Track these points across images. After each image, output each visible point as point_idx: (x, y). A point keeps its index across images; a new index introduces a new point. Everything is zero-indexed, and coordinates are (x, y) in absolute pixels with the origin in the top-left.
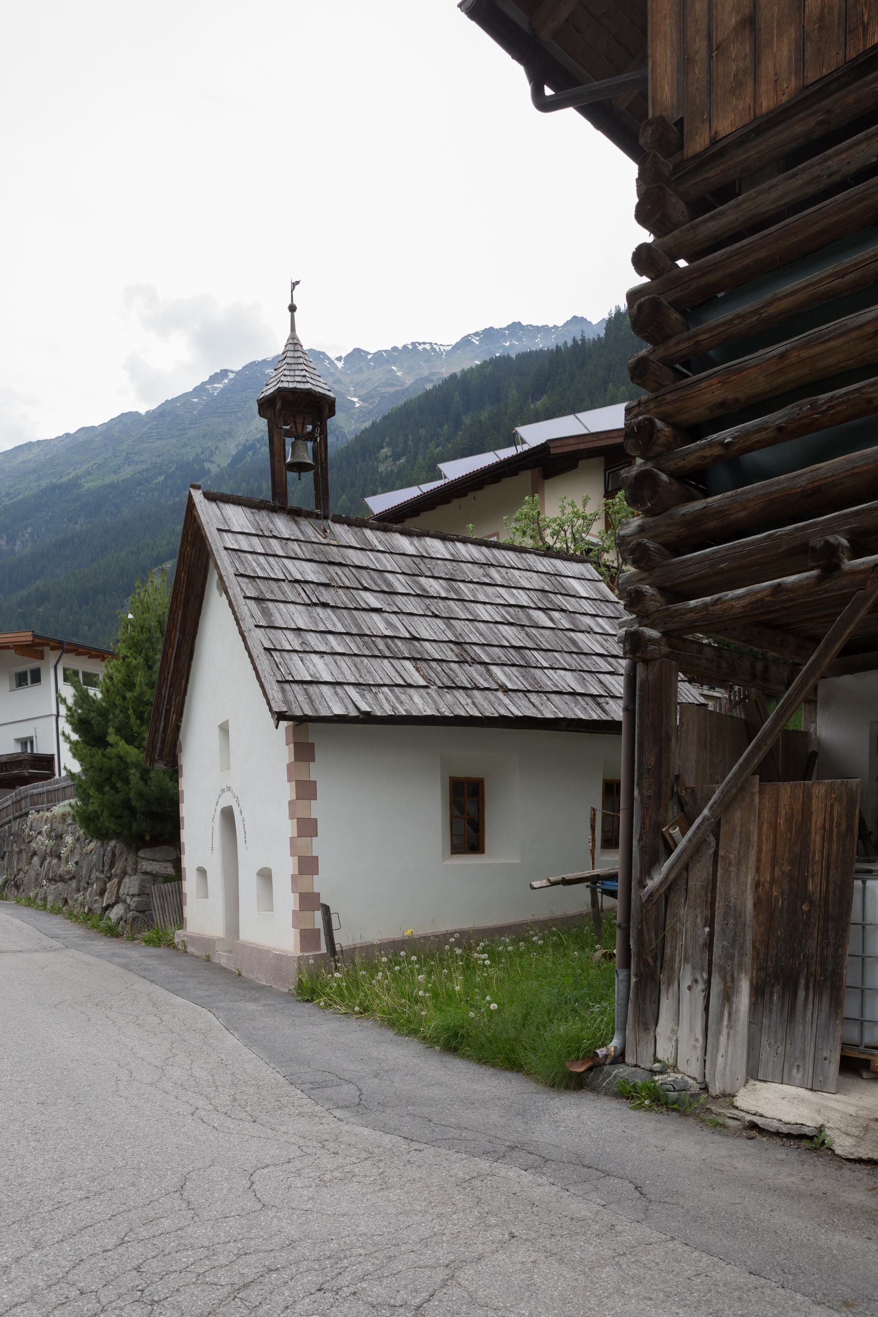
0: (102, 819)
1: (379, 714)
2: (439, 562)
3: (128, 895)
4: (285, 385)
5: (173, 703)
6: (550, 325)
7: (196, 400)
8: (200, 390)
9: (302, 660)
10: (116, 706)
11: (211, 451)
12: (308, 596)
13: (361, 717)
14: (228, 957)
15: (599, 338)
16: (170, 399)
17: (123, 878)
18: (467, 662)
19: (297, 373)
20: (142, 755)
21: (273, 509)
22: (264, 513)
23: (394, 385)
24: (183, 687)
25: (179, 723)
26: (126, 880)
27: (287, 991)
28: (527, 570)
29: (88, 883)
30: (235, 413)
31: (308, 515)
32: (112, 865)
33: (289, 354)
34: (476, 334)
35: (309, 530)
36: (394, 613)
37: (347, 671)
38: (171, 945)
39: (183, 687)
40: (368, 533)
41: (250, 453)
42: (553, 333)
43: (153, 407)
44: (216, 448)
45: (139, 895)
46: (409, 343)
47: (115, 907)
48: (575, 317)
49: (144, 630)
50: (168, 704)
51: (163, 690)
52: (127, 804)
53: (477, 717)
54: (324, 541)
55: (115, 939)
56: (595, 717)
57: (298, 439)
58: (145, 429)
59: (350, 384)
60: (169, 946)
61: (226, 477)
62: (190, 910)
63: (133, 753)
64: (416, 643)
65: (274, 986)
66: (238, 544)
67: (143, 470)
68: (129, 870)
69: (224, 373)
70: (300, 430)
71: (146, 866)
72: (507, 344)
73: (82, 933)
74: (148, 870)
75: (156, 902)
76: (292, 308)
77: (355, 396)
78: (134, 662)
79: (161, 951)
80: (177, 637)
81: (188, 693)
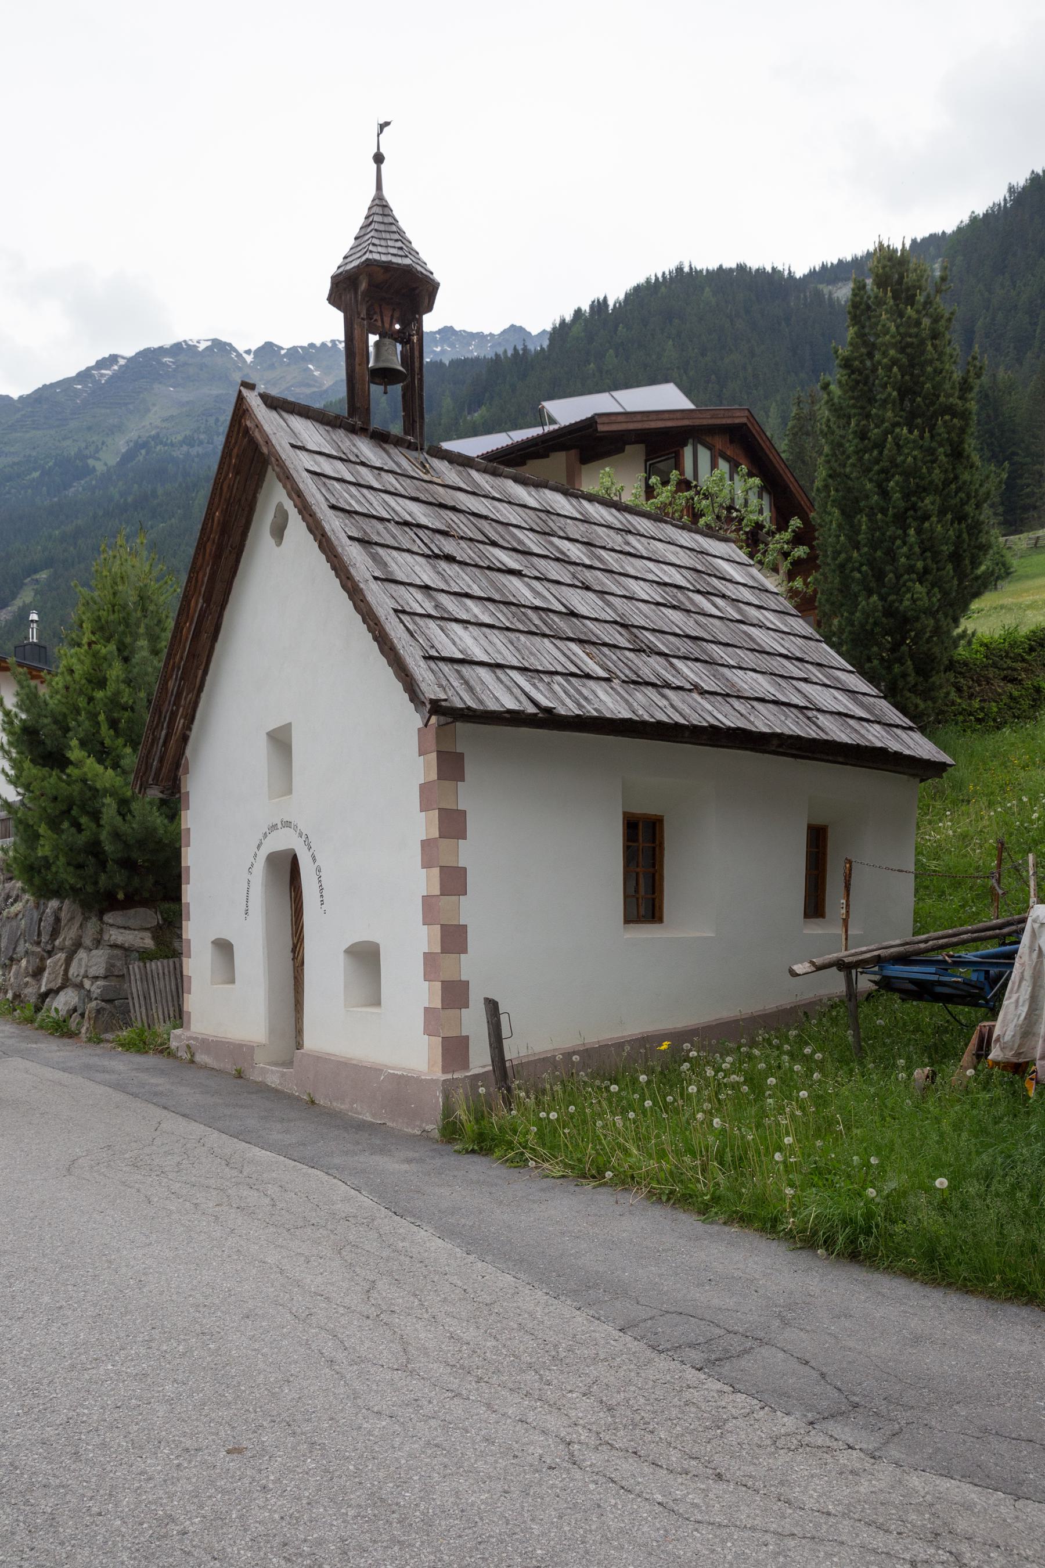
0: (54, 869)
1: (563, 713)
2: (569, 521)
3: (86, 976)
4: (376, 257)
5: (183, 702)
6: (486, 332)
7: (79, 387)
8: (84, 376)
9: (442, 630)
10: (78, 712)
12: (426, 544)
13: (540, 715)
14: (283, 1075)
15: (542, 349)
16: (48, 383)
17: (75, 952)
18: (644, 651)
19: (390, 243)
20: (118, 778)
21: (352, 430)
22: (341, 433)
23: (308, 385)
24: (198, 680)
25: (188, 732)
26: (82, 954)
27: (419, 1133)
28: (669, 543)
29: (11, 959)
31: (398, 442)
32: (55, 933)
33: (377, 218)
35: (402, 460)
36: (536, 578)
37: (500, 649)
38: (164, 1050)
39: (198, 680)
40: (474, 473)
41: (143, 452)
42: (489, 341)
43: (27, 390)
44: (103, 443)
45: (105, 977)
47: (62, 993)
48: (513, 326)
50: (174, 704)
51: (171, 684)
52: (94, 848)
53: (683, 725)
54: (426, 477)
55: (67, 1040)
56: (815, 736)
58: (18, 416)
60: (161, 1052)
61: (114, 477)
62: (192, 1002)
63: (105, 777)
64: (575, 620)
65: (389, 1124)
66: (319, 466)
67: (14, 464)
68: (87, 941)
69: (114, 358)
70: (387, 325)
72: (438, 349)
73: (12, 1030)
74: (119, 942)
75: (135, 987)
76: (379, 159)
78: (104, 651)
79: (150, 1060)
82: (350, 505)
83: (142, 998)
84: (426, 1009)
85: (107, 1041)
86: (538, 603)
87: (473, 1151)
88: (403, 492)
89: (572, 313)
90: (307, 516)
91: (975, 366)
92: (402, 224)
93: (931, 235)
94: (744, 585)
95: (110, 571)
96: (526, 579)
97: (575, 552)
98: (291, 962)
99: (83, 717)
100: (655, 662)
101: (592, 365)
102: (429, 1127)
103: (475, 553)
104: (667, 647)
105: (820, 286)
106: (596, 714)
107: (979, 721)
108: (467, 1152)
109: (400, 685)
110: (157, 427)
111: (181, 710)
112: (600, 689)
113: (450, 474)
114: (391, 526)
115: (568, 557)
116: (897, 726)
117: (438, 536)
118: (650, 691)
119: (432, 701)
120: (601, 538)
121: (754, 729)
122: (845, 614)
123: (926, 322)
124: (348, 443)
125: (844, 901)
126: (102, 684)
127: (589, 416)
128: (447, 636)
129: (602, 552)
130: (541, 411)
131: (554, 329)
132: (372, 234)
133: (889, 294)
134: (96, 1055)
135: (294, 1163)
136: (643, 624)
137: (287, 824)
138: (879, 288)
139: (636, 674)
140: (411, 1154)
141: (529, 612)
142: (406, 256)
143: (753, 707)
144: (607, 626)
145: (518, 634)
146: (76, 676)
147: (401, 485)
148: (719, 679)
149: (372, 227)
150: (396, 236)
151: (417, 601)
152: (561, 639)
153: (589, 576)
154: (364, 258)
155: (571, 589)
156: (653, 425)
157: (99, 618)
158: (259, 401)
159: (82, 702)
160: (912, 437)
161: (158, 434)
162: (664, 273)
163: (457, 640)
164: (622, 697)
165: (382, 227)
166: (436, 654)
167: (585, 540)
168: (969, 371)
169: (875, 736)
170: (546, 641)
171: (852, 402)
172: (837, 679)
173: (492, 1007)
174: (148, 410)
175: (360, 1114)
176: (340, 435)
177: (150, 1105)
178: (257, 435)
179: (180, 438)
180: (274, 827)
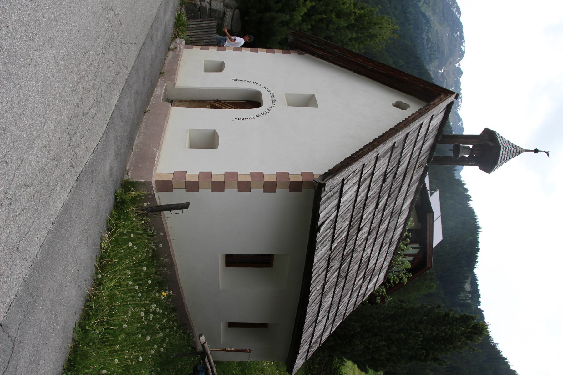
2: (396, 221)
4: (502, 150)
5: (329, 55)
9: (355, 183)
11: (428, 4)
13: (317, 227)
14: (160, 96)
15: (455, 176)
18: (342, 260)
19: (506, 155)
20: (298, 21)
21: (437, 137)
28: (385, 259)
30: (443, 16)
31: (431, 155)
33: (515, 150)
34: (462, 124)
36: (374, 214)
38: (175, 36)
40: (417, 184)
41: (425, 21)
44: (429, 6)
45: (210, 9)
46: (462, 96)
49: (369, 24)
51: (337, 51)
54: (417, 167)
57: (471, 151)
59: (449, 69)
60: (175, 34)
62: (197, 51)
65: (132, 153)
69: (460, 13)
71: (229, 14)
74: (226, 15)
76: (536, 151)
77: (444, 70)
78: (352, 18)
79: (171, 29)
80: (369, 67)
81: (334, 65)
82: (408, 140)
83: (200, 25)
84: (186, 172)
85: (181, 9)
86: (364, 217)
87: (116, 199)
88: (411, 159)
89: (467, 188)
90: (404, 123)
91: (443, 363)
92: (512, 160)
93: (484, 317)
94: (367, 288)
95: (384, 22)
96: (374, 210)
97: (384, 226)
98: (213, 99)
99: (325, 8)
100: (338, 264)
101: (448, 195)
102: (130, 174)
103: (386, 190)
104: (343, 268)
105: (470, 279)
106: (316, 248)
107: (310, 367)
108: (116, 196)
109: (332, 168)
110: (434, 28)
111: (326, 54)
112: (327, 247)
113: (417, 176)
114: (399, 157)
115: (382, 224)
116: (308, 354)
117: (393, 175)
118: (326, 265)
119: (324, 185)
120: (389, 235)
121: (308, 307)
122: (353, 318)
123: (459, 344)
124: (432, 136)
125: (233, 350)
126: (338, 16)
127: (433, 210)
128: (352, 185)
129: (383, 236)
130: (436, 190)
131: (462, 181)
132: (510, 148)
133: (470, 330)
134: (174, 4)
135: (110, 116)
136: (353, 257)
137: (274, 103)
138: (473, 326)
139: (333, 259)
140: (115, 169)
141: (361, 214)
142: (501, 162)
143: (317, 304)
144: (353, 244)
145: (351, 212)
146: (342, 6)
147: (414, 158)
148: (329, 289)
149: (512, 148)
150: (508, 158)
151: (367, 172)
152: (349, 228)
153: (374, 233)
154: (501, 145)
155: (369, 227)
156: (428, 234)
157: (365, 16)
158: (451, 101)
159: (331, 7)
160: (419, 342)
161: (432, 28)
162: (478, 222)
163: (351, 189)
164: (323, 256)
165: (512, 152)
166: (345, 182)
167: (388, 229)
168: (441, 361)
169: (303, 349)
170: (349, 223)
171: (433, 317)
172: (328, 328)
173: (185, 206)
174: (440, 24)
175: (138, 138)
176: (435, 132)
177: (145, 36)
178: (437, 100)
179: (430, 36)
180: (273, 96)
